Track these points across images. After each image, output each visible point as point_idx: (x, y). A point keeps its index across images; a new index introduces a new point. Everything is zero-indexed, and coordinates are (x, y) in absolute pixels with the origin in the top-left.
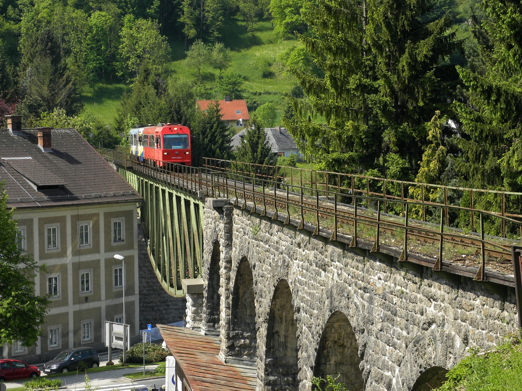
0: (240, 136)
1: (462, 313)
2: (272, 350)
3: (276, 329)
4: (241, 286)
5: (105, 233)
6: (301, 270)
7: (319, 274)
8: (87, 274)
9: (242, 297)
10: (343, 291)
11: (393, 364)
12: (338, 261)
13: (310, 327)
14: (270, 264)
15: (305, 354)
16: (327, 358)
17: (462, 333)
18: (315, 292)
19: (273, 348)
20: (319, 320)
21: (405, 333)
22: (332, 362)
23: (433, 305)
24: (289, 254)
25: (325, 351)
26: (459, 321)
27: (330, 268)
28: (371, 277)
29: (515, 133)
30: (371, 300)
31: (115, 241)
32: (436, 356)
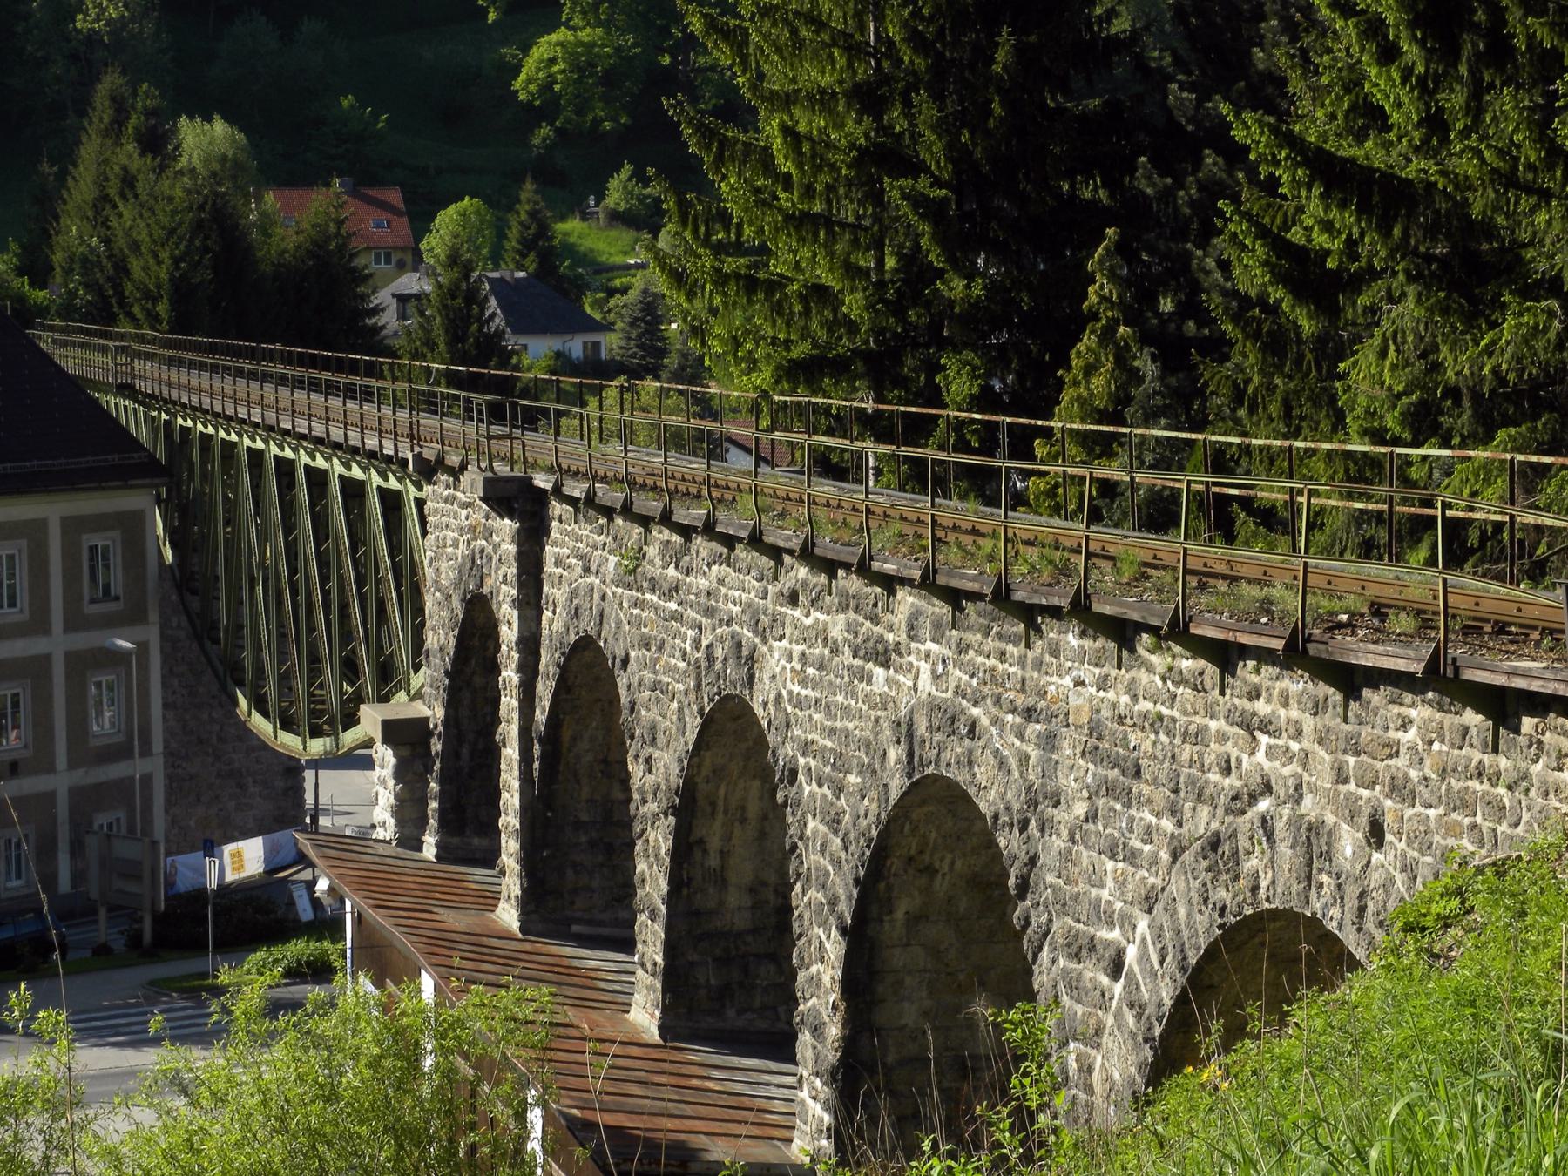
0: (394, 296)
1: (1359, 765)
2: (685, 891)
3: (698, 833)
4: (568, 717)
5: (64, 577)
6: (798, 667)
7: (868, 678)
8: (16, 695)
9: (570, 750)
10: (953, 720)
11: (1127, 908)
12: (933, 640)
13: (834, 822)
14: (685, 653)
15: (815, 895)
16: (888, 905)
17: (1364, 820)
18: (851, 726)
19: (688, 885)
20: (866, 802)
21: (1167, 824)
22: (900, 915)
23: (1263, 749)
24: (755, 626)
25: (882, 885)
26: (1352, 787)
27: (903, 661)
28: (1048, 679)
29: (1389, 290)
30: (1049, 742)
31: (93, 601)
32: (1273, 882)
